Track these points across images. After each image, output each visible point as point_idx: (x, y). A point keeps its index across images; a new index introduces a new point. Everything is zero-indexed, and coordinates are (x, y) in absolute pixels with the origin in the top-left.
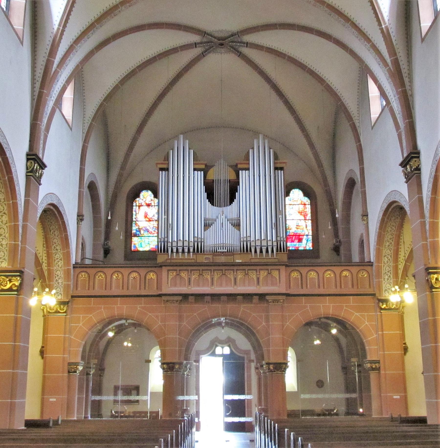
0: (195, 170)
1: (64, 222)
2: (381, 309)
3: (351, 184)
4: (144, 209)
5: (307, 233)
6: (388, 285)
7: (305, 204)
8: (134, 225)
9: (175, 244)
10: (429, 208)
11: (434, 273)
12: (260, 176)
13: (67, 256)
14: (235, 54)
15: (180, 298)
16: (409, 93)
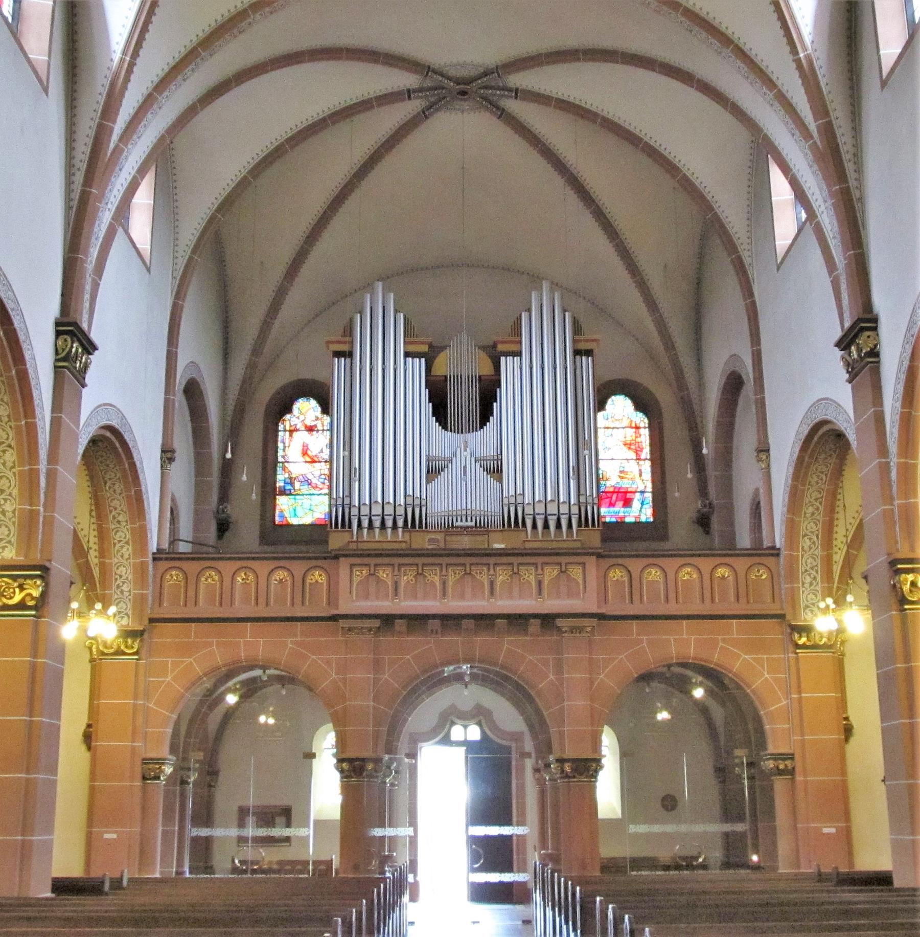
0: (407, 355)
1: (133, 465)
2: (797, 646)
3: (734, 385)
4: (301, 437)
5: (641, 488)
6: (811, 596)
7: (637, 428)
8: (279, 470)
9: (365, 511)
10: (896, 435)
11: (908, 571)
12: (543, 369)
13: (141, 535)
14: (492, 112)
15: (377, 623)
16: (856, 194)
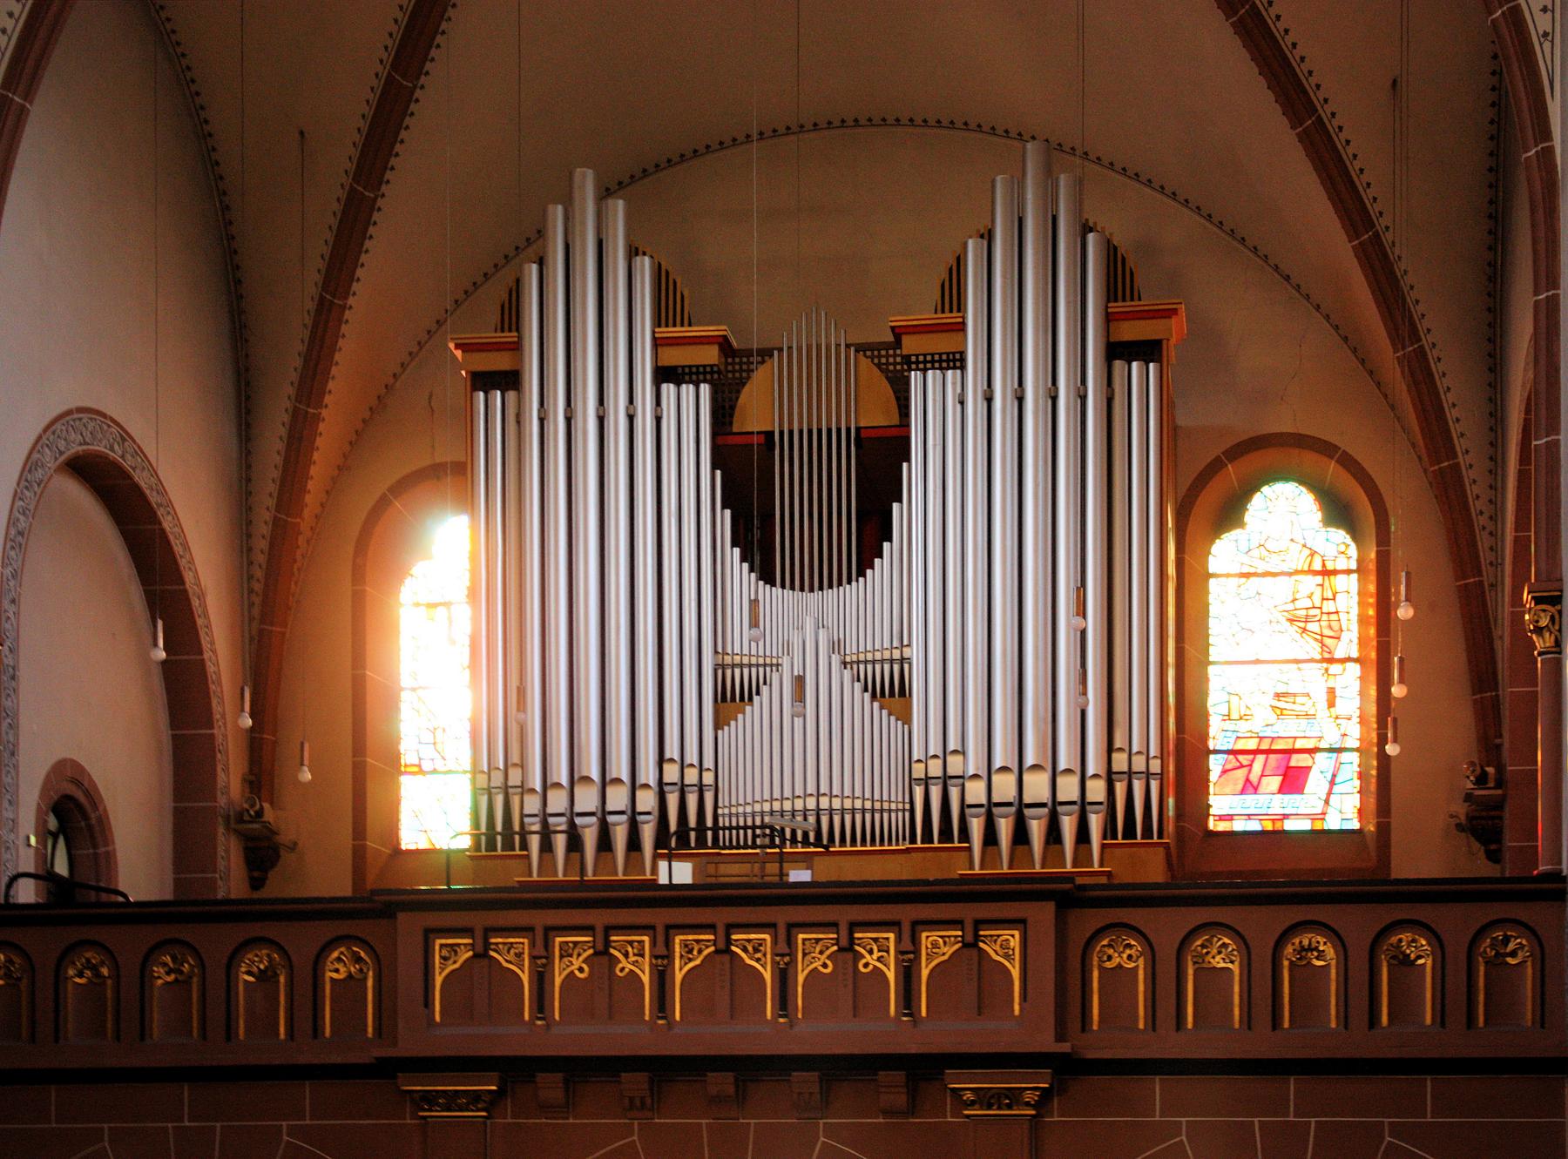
0: (664, 375)
5: (1332, 739)
12: (989, 400)
